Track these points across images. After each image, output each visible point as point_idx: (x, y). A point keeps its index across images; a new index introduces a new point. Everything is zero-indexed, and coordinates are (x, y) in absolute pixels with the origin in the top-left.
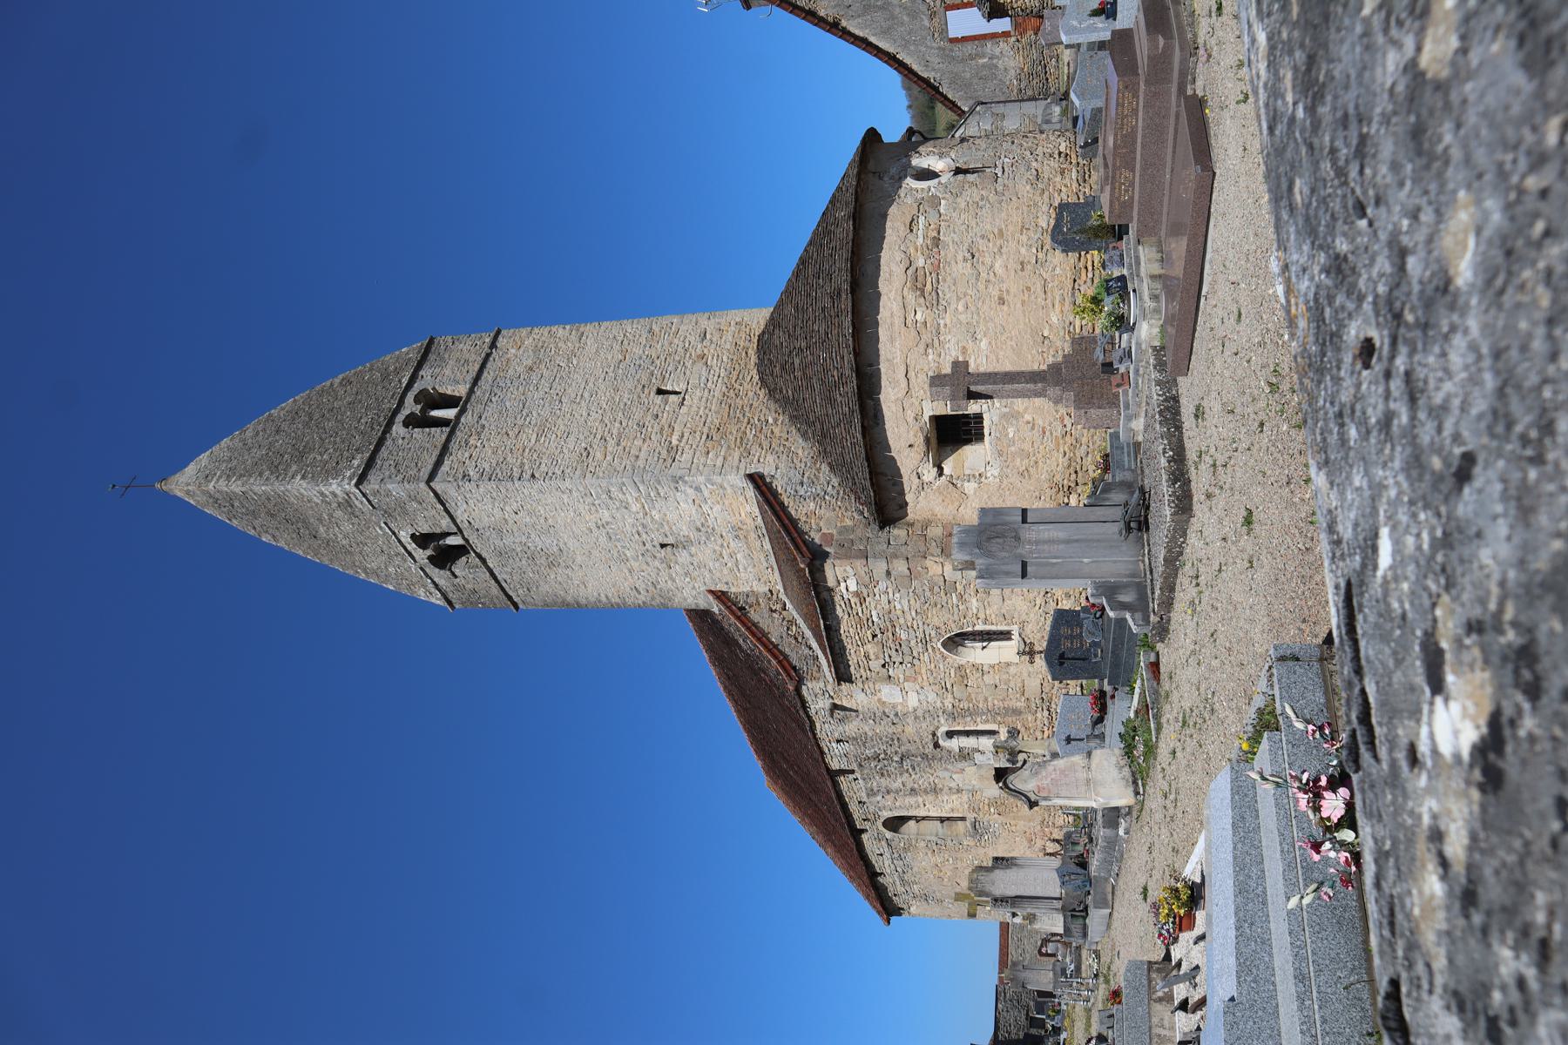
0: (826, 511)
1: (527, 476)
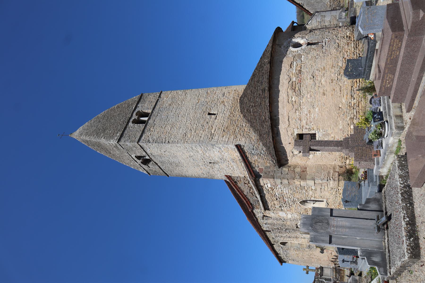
0: (262, 161)
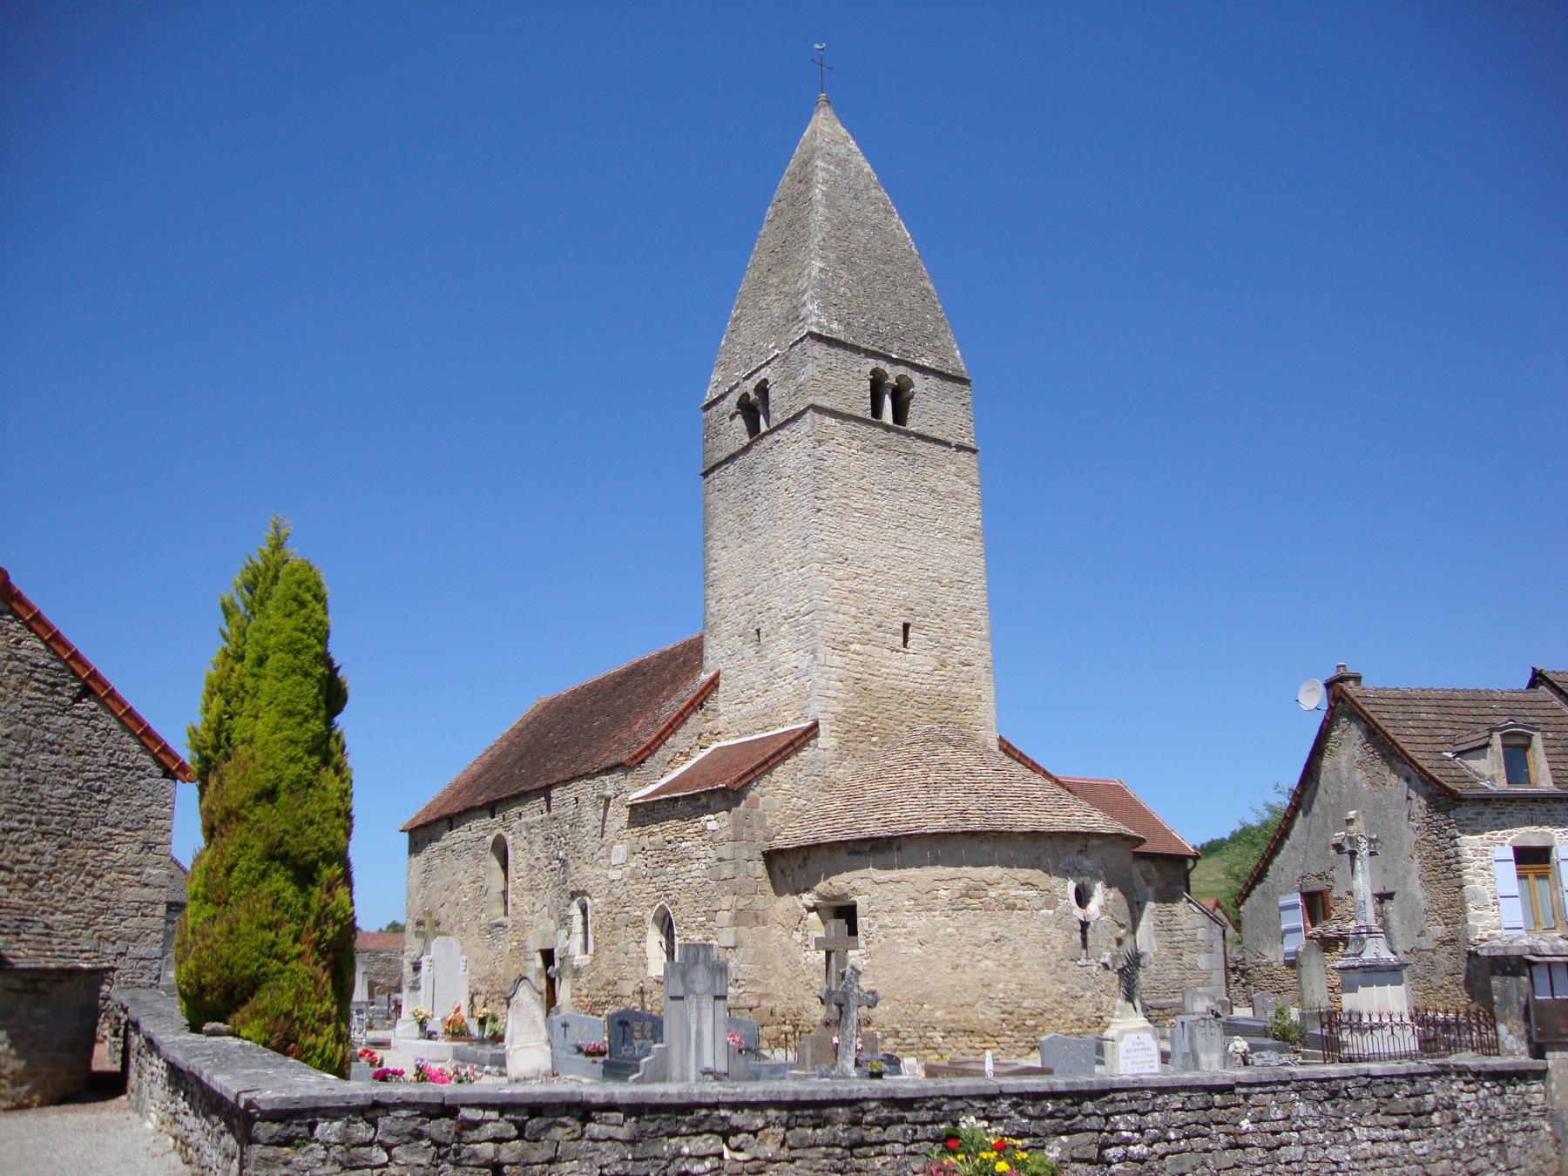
1: (819, 504)
